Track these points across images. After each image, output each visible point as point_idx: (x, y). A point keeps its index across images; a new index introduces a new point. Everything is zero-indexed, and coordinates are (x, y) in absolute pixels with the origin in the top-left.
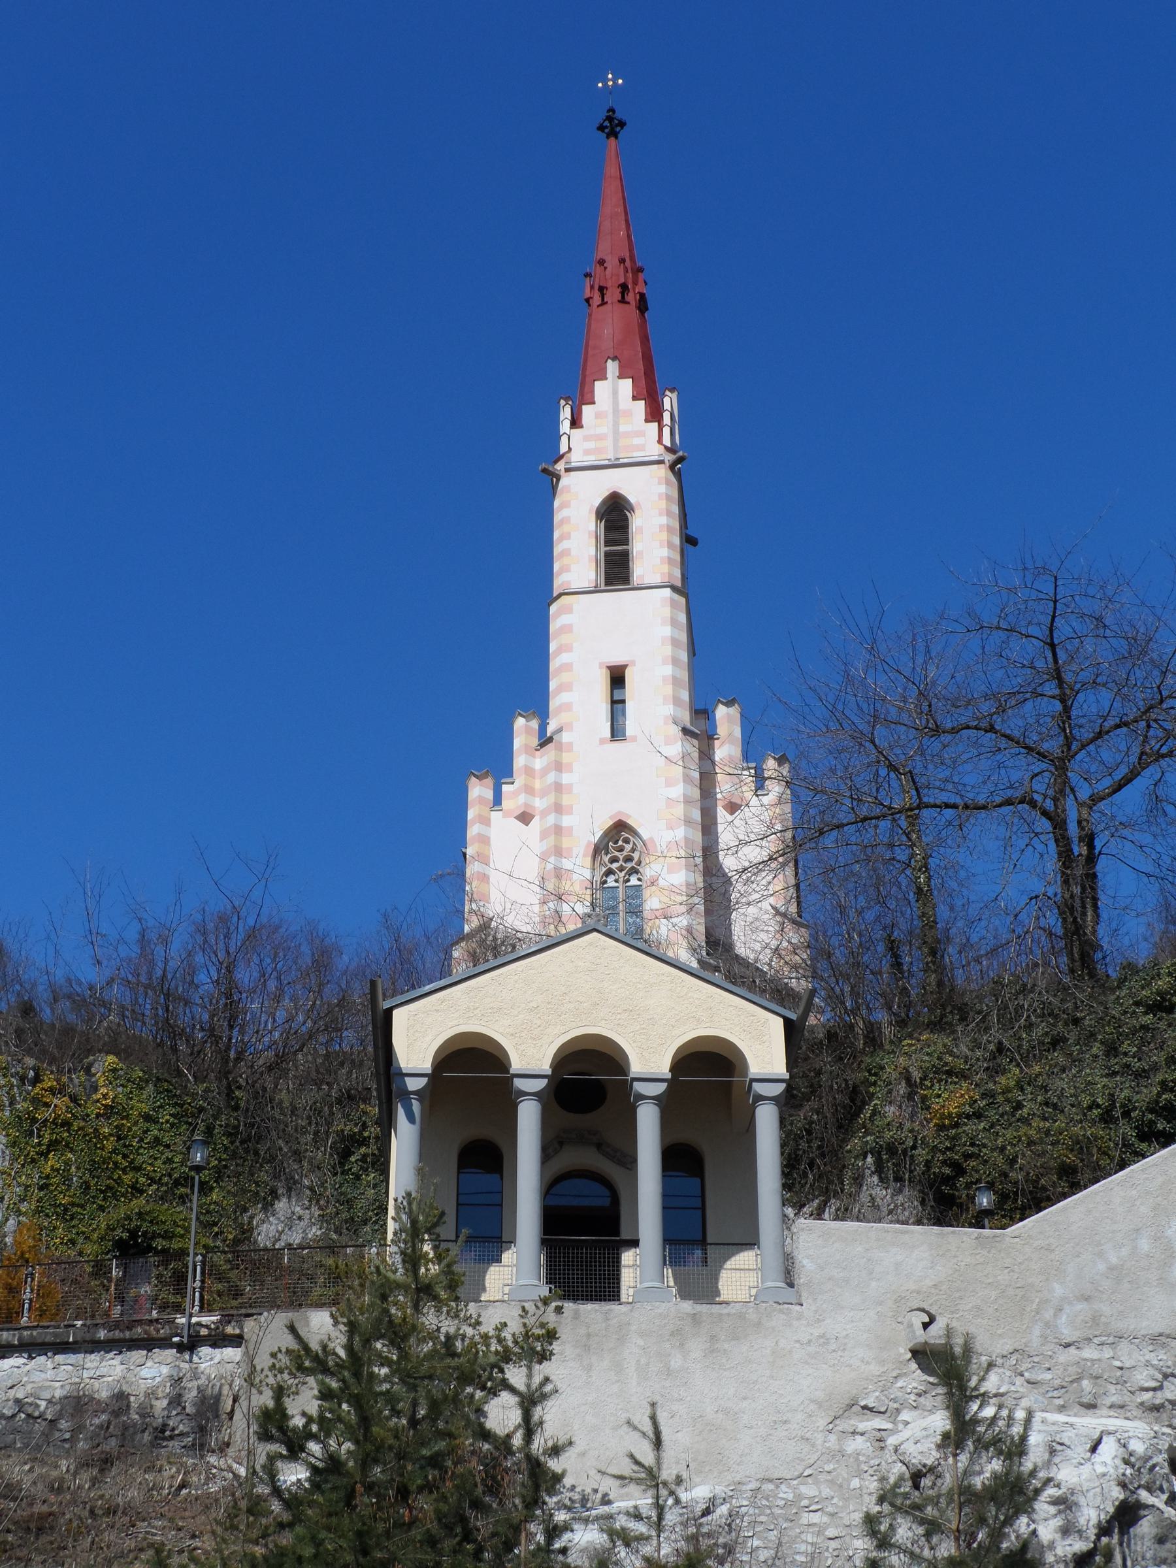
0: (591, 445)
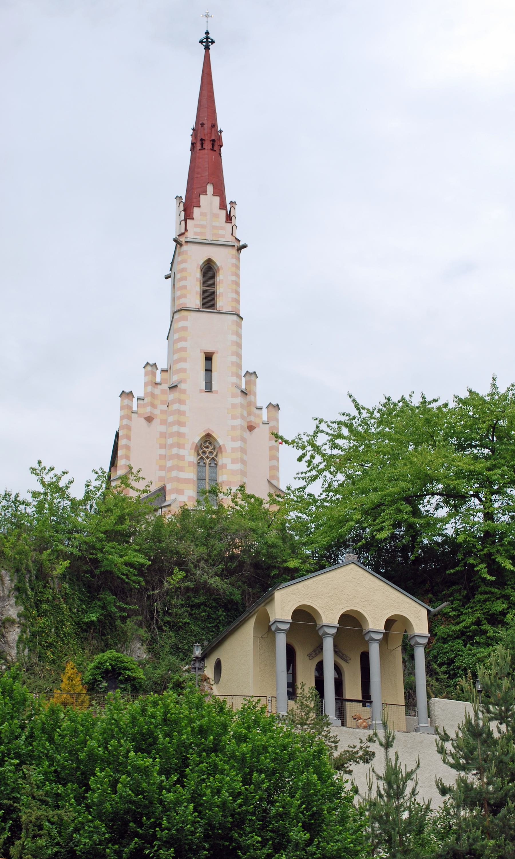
0: (198, 230)
